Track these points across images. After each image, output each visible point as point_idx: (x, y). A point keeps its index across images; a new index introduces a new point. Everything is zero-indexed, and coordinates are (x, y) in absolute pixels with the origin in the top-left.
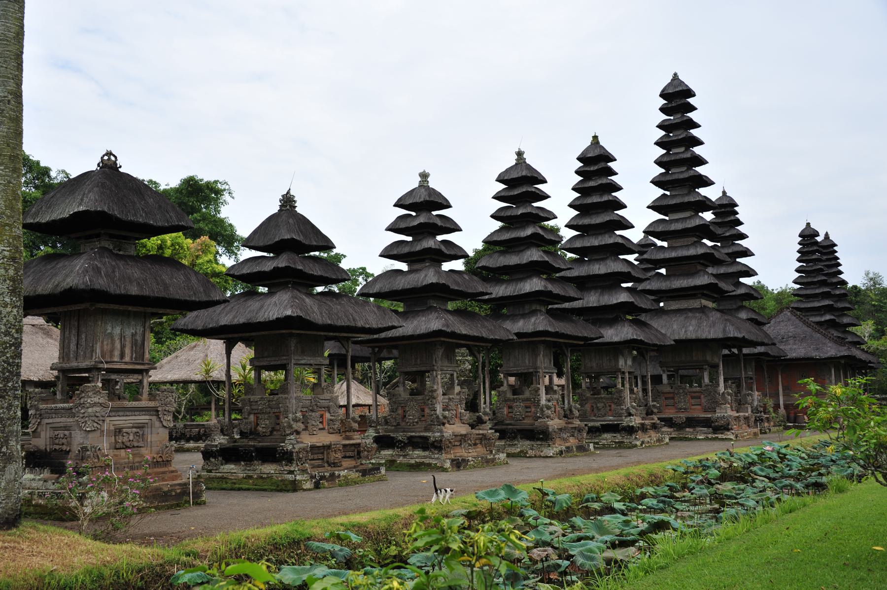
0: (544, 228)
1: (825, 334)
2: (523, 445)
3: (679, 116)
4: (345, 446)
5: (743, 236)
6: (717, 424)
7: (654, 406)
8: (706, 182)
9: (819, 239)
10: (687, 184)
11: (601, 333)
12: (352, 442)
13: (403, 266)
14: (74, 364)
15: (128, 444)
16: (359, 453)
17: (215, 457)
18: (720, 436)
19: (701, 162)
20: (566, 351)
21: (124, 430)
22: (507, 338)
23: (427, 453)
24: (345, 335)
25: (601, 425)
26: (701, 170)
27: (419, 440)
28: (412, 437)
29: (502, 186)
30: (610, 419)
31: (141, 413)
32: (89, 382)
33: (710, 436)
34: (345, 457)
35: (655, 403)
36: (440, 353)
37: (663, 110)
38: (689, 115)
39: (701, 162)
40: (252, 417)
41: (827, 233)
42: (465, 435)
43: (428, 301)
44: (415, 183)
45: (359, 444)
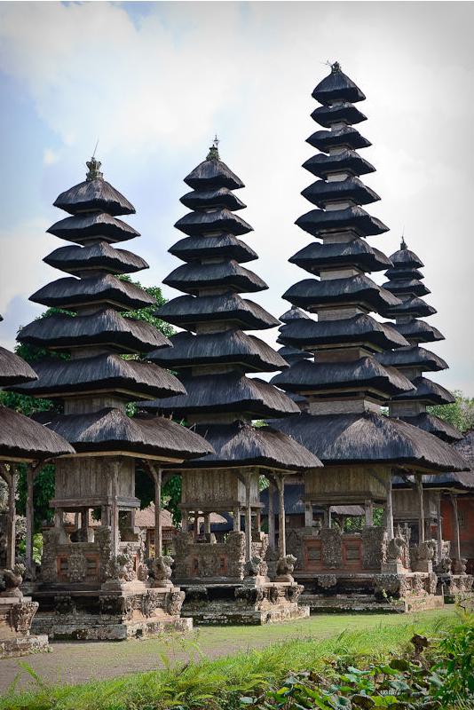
7: (289, 560)
25: (208, 589)
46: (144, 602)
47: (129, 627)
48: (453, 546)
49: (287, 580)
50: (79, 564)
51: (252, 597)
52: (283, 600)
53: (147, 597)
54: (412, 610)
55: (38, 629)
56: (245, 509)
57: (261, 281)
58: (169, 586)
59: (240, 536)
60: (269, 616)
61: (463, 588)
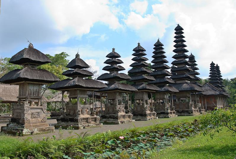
0: (145, 62)
2: (139, 117)
3: (179, 35)
4: (92, 118)
5: (196, 65)
8: (187, 51)
9: (215, 66)
12: (94, 117)
13: (108, 72)
14: (22, 97)
15: (35, 117)
17: (60, 121)
19: (185, 46)
21: (34, 113)
23: (114, 120)
24: (92, 90)
26: (185, 48)
28: (110, 116)
29: (134, 52)
30: (163, 111)
31: (33, 109)
32: (25, 101)
36: (118, 94)
37: (175, 33)
38: (182, 34)
39: (185, 46)
40: (69, 110)
42: (124, 115)
44: (111, 51)
45: (96, 118)
51: (168, 113)
52: (173, 114)
56: (166, 99)
58: (154, 112)
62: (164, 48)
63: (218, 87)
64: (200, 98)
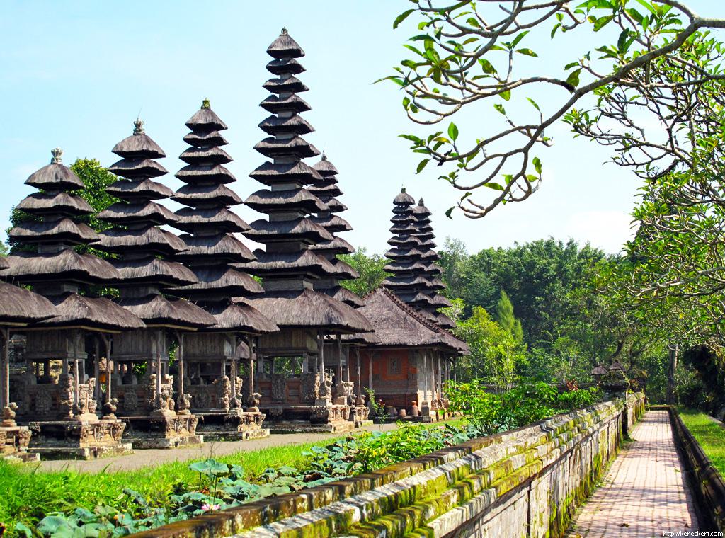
1: (398, 302)
6: (315, 416)
7: (256, 396)
8: (307, 151)
10: (292, 153)
11: (215, 319)
16: (18, 439)
18: (318, 429)
20: (179, 338)
22: (138, 326)
23: (62, 442)
25: (204, 416)
27: (54, 429)
28: (46, 426)
30: (213, 412)
33: (307, 429)
34: (7, 443)
35: (257, 394)
37: (271, 68)
41: (421, 199)
43: (62, 287)
45: (17, 432)
46: (96, 428)
47: (171, 440)
48: (356, 385)
49: (254, 411)
50: (132, 399)
51: (236, 421)
52: (253, 424)
53: (178, 421)
54: (336, 431)
55: (125, 438)
56: (230, 361)
57: (239, 198)
58: (188, 413)
59: (225, 380)
60: (247, 435)
61: (363, 416)
62: (308, 102)
63: (424, 305)
64: (352, 356)
